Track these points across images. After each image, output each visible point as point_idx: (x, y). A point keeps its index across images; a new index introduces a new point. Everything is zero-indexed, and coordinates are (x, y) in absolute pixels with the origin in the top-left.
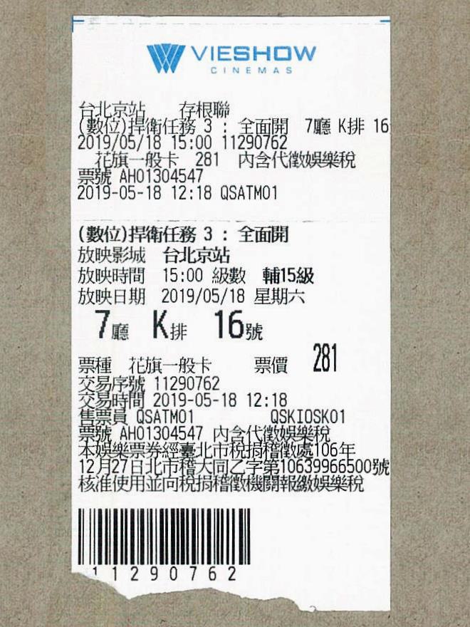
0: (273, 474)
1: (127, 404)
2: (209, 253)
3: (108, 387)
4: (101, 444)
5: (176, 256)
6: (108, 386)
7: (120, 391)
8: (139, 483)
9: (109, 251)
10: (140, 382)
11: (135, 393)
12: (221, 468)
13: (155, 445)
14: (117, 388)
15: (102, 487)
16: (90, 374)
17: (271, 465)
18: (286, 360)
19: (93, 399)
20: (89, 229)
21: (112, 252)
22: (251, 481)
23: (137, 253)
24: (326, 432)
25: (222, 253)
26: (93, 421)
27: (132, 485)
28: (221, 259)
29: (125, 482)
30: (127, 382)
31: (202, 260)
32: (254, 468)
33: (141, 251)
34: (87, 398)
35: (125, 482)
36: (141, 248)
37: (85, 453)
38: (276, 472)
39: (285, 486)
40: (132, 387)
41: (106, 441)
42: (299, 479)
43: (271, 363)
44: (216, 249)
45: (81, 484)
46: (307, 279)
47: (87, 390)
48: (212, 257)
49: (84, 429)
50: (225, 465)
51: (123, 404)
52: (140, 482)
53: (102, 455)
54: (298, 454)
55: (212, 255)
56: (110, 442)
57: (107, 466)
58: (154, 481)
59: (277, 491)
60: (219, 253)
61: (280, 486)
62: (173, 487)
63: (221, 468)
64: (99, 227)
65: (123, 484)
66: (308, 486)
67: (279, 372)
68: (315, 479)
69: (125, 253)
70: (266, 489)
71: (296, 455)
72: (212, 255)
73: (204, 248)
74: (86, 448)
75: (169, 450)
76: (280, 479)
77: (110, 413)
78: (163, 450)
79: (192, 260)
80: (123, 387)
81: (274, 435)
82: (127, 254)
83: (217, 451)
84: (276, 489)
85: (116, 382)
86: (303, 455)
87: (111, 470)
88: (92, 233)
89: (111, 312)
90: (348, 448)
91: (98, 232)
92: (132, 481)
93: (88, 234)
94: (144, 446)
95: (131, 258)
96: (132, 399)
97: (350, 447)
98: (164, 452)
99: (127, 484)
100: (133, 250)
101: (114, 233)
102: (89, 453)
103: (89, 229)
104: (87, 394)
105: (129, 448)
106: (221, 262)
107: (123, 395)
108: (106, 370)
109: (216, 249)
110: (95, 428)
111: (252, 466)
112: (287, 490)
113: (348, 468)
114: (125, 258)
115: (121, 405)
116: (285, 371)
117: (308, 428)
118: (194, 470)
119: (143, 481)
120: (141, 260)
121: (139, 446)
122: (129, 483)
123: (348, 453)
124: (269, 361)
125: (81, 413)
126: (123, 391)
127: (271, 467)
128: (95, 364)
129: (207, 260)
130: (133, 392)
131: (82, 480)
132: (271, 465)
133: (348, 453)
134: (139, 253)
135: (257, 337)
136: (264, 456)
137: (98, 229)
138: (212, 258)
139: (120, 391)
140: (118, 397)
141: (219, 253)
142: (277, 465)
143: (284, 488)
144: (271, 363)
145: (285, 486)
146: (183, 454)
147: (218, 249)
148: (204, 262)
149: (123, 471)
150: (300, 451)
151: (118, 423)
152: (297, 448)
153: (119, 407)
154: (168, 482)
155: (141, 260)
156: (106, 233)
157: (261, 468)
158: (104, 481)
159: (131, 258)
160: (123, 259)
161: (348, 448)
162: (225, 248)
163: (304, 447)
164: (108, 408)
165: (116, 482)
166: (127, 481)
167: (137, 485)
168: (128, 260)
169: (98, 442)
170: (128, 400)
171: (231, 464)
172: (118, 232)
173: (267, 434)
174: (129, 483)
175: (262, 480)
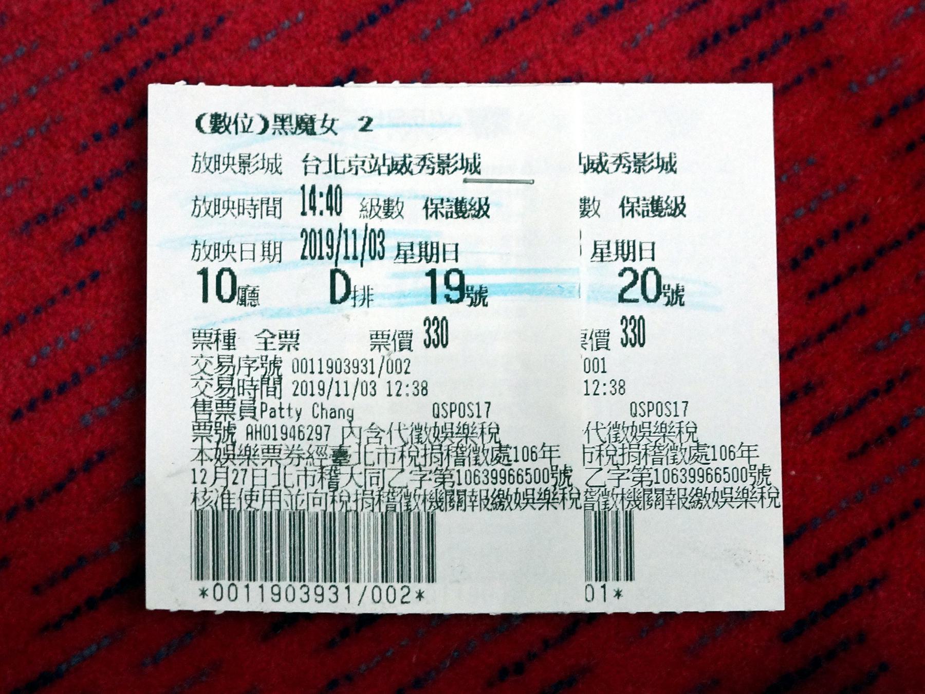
0: (645, 487)
1: (258, 392)
2: (364, 162)
3: (231, 372)
4: (222, 446)
5: (317, 166)
6: (231, 368)
7: (248, 376)
8: (274, 498)
9: (233, 158)
10: (276, 364)
11: (269, 379)
12: (374, 480)
13: (296, 448)
14: (244, 371)
15: (223, 503)
16: (207, 352)
17: (444, 475)
18: (411, 334)
19: (211, 385)
20: (212, 116)
21: (237, 160)
22: (625, 496)
23: (271, 161)
24: (495, 431)
25: (380, 162)
26: (210, 414)
27: (264, 501)
28: (379, 170)
29: (254, 498)
30: (258, 364)
31: (354, 171)
32: (619, 479)
33: (276, 159)
34: (202, 384)
35: (254, 498)
36: (276, 155)
37: (200, 458)
38: (649, 483)
39: (475, 504)
40: (264, 370)
41: (229, 442)
42: (493, 493)
43: (391, 338)
44: (373, 157)
45: (195, 500)
46: (482, 213)
47: (202, 374)
48: (367, 167)
49: (199, 426)
50: (381, 475)
51: (252, 392)
52: (276, 498)
53: (223, 461)
54: (492, 461)
55: (367, 165)
56: (234, 444)
57: (225, 475)
58: (294, 497)
59: (662, 509)
60: (377, 161)
61: (468, 503)
62: (320, 505)
63: (374, 480)
64: (225, 114)
65: (251, 500)
66: (506, 504)
67: (598, 349)
68: (715, 492)
69: (649, 160)
70: (449, 508)
71: (489, 463)
72: (367, 165)
73: (357, 156)
74: (201, 451)
75: (315, 455)
76: (665, 493)
77: (234, 404)
78: (307, 455)
79: (340, 170)
80: (252, 369)
81: (621, 436)
82: (257, 162)
83: (382, 457)
84: (463, 508)
85: (242, 364)
86: (499, 462)
87: (230, 481)
88: (216, 121)
89: (300, 258)
90: (551, 451)
91: (224, 120)
92: (264, 496)
93: (211, 122)
94: (280, 450)
95: (263, 168)
96: (265, 387)
97: (553, 449)
98: (307, 458)
99: (257, 500)
100: (266, 157)
101: (247, 122)
102: (205, 458)
103: (212, 116)
104: (202, 379)
105: (259, 452)
106: (380, 174)
107: (252, 381)
108: (229, 346)
109: (373, 157)
110: (213, 424)
111: (616, 476)
112: (675, 507)
113: (723, 476)
114: (255, 168)
115: (250, 394)
116: (410, 349)
117: (471, 424)
118: (338, 483)
119: (280, 496)
120: (277, 171)
121: (274, 449)
122: (261, 498)
123: (551, 458)
124: (389, 335)
125: (195, 405)
126: (251, 376)
127: (444, 478)
128: (214, 337)
129: (360, 171)
130: (266, 376)
131: (195, 493)
132: (642, 474)
133: (551, 458)
134: (273, 161)
135: (678, 302)
136: (643, 462)
137: (225, 116)
138: (368, 170)
139: (248, 376)
140: (246, 383)
141: (377, 161)
142: (452, 475)
143: (473, 506)
144: (391, 338)
145: (475, 504)
146: (334, 461)
147: (375, 156)
148: (356, 173)
149: (298, 485)
150: (495, 456)
151: (245, 418)
152: (490, 452)
153: (246, 397)
154: (314, 498)
155: (277, 171)
156: (236, 122)
157: (628, 479)
158: (226, 496)
159: (263, 168)
160: (647, 168)
161: (551, 451)
162: (384, 155)
163: (500, 451)
164: (233, 399)
165: (243, 496)
166: (257, 496)
167: (271, 501)
168: (458, 171)
169: (218, 443)
170: (259, 387)
171: (389, 475)
172: (251, 121)
173: (415, 433)
174: (261, 498)
175: (444, 495)
